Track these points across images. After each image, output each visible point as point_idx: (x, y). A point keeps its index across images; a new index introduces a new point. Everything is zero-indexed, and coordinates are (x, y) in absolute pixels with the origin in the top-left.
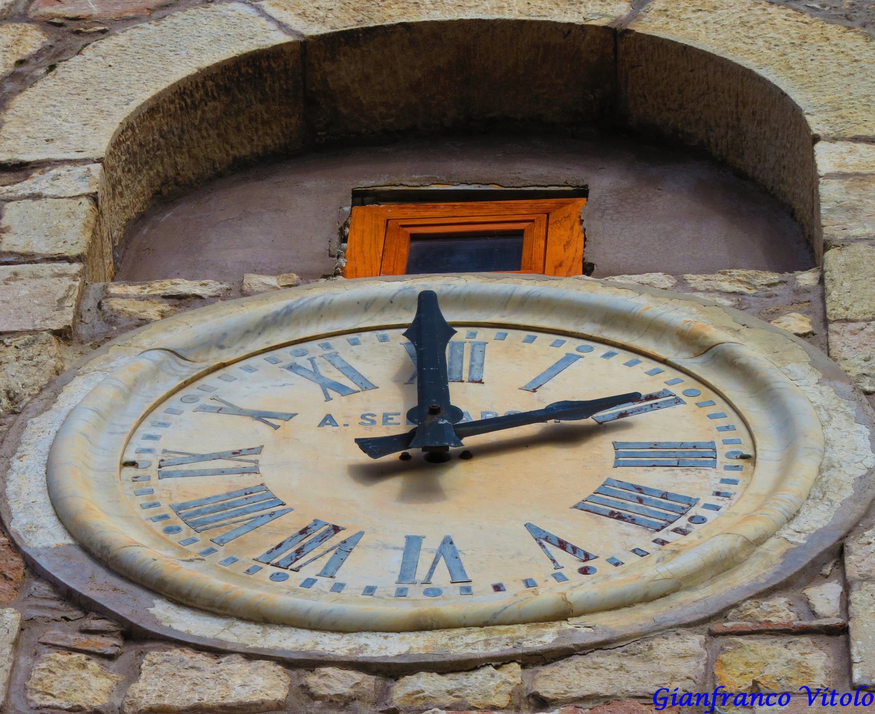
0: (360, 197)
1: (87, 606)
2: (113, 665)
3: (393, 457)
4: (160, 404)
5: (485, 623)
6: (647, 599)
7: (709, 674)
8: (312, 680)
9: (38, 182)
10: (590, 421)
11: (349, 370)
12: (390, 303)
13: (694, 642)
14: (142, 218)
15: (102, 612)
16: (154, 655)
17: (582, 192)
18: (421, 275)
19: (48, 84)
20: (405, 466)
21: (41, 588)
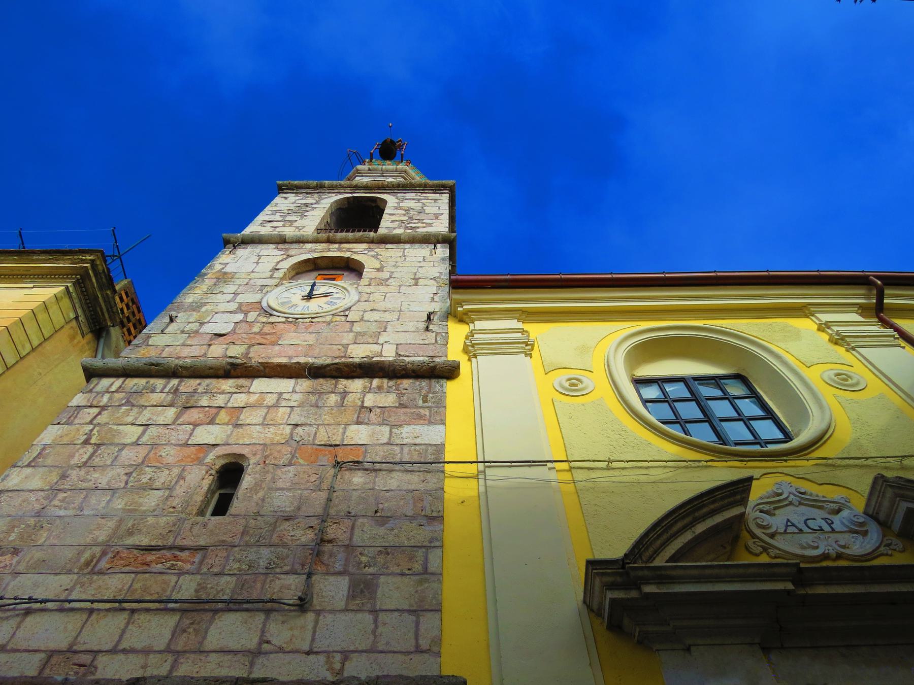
0: (319, 275)
1: (267, 312)
2: (753, 518)
3: (306, 298)
4: (808, 447)
5: (308, 314)
6: (327, 312)
7: (331, 320)
8: (288, 320)
9: (280, 271)
10: (329, 294)
11: (305, 289)
12: (309, 283)
13: (331, 316)
14: (294, 276)
15: (268, 313)
16: (272, 317)
17: (343, 275)
18: (661, 360)
19: (285, 261)
20: (307, 299)
21: (263, 310)
